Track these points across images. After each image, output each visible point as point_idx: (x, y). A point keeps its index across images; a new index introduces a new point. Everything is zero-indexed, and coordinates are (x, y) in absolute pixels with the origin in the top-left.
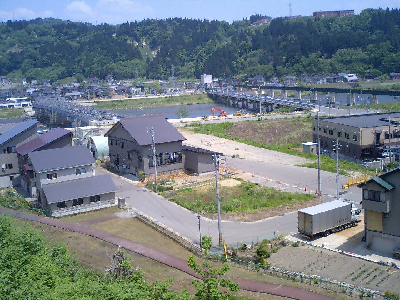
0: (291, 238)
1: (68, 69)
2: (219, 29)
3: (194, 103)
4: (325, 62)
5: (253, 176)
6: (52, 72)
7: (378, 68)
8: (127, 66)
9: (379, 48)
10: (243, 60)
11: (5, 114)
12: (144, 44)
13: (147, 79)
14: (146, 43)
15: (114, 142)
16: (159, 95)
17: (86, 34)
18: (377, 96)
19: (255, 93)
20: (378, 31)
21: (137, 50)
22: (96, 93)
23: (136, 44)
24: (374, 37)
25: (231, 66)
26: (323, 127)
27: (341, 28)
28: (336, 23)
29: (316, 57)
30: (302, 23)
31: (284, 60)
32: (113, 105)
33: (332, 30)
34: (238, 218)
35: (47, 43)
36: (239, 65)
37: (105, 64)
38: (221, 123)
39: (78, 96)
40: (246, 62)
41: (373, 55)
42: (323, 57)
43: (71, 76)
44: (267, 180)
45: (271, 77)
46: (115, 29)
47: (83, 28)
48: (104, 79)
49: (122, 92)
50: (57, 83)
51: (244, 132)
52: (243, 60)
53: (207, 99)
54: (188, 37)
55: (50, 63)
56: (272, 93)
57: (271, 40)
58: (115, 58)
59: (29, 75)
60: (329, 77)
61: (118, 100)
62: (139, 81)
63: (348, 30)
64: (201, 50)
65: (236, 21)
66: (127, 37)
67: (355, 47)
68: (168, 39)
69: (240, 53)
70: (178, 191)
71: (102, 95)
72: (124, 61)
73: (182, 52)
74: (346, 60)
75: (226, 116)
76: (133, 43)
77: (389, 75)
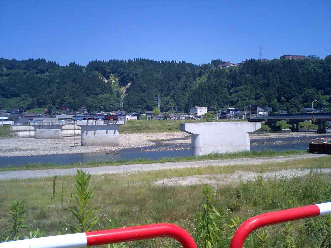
12: (113, 82)
14: (115, 80)
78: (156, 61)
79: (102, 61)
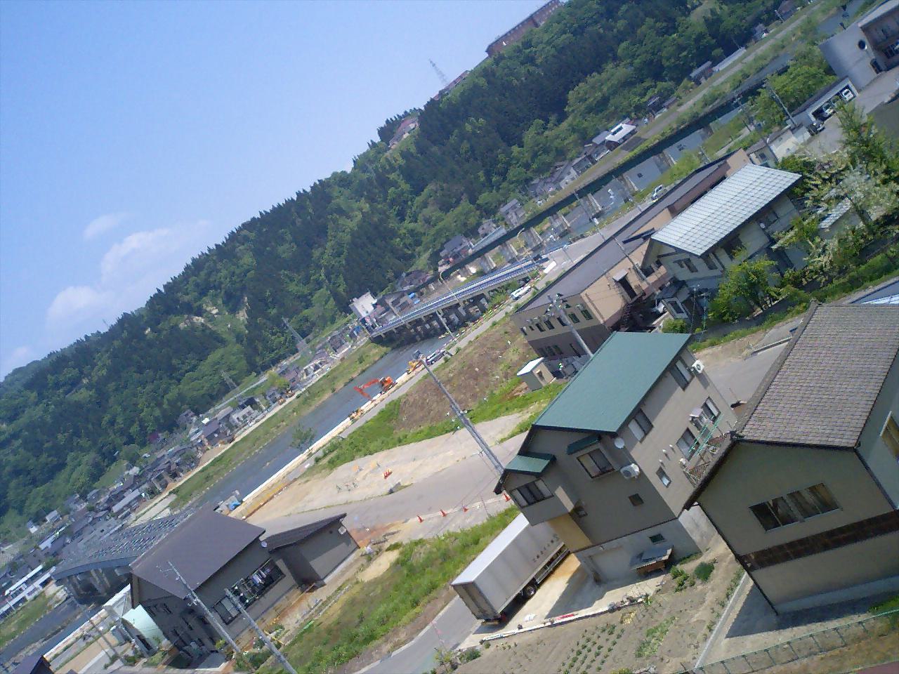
0: (471, 641)
1: (100, 451)
2: (335, 194)
3: (355, 375)
4: (560, 132)
5: (421, 521)
6: (74, 476)
7: (663, 80)
8: (207, 373)
9: (641, 42)
10: (412, 225)
11: (12, 628)
12: (215, 311)
13: (258, 374)
14: (215, 305)
15: (154, 609)
16: (285, 401)
17: (95, 361)
18: (665, 151)
19: (459, 281)
20: (624, 8)
21: (208, 331)
22: (168, 470)
23: (199, 320)
24: (621, 24)
25: (393, 251)
26: (533, 323)
27: (554, 46)
28: (538, 43)
29: (538, 134)
30: (476, 86)
31: (482, 179)
32: (208, 478)
33: (539, 61)
34: (389, 646)
35: (31, 426)
36: (408, 241)
37: (163, 397)
38: (379, 413)
39: (139, 498)
40: (419, 226)
41: (637, 61)
42: (550, 125)
43: (114, 460)
44: (444, 515)
45: (479, 224)
46: (143, 316)
47: (83, 353)
48: (178, 427)
49: (216, 435)
50: (95, 491)
51: (422, 408)
52: (412, 225)
53: (377, 351)
54: (286, 246)
55: (61, 461)
56: (487, 263)
57: (439, 153)
58: (174, 374)
59: (34, 509)
60: (577, 161)
61: (210, 461)
62: (241, 393)
63: (567, 42)
64: (324, 254)
65: (357, 158)
66: (174, 319)
67: (598, 68)
68: (251, 274)
69: (397, 215)
70: (293, 644)
71: (183, 468)
72: (194, 368)
73: (292, 280)
74: (595, 102)
75: (393, 385)
76: (192, 323)
77: (690, 79)
78: (373, 145)
79: (171, 281)
